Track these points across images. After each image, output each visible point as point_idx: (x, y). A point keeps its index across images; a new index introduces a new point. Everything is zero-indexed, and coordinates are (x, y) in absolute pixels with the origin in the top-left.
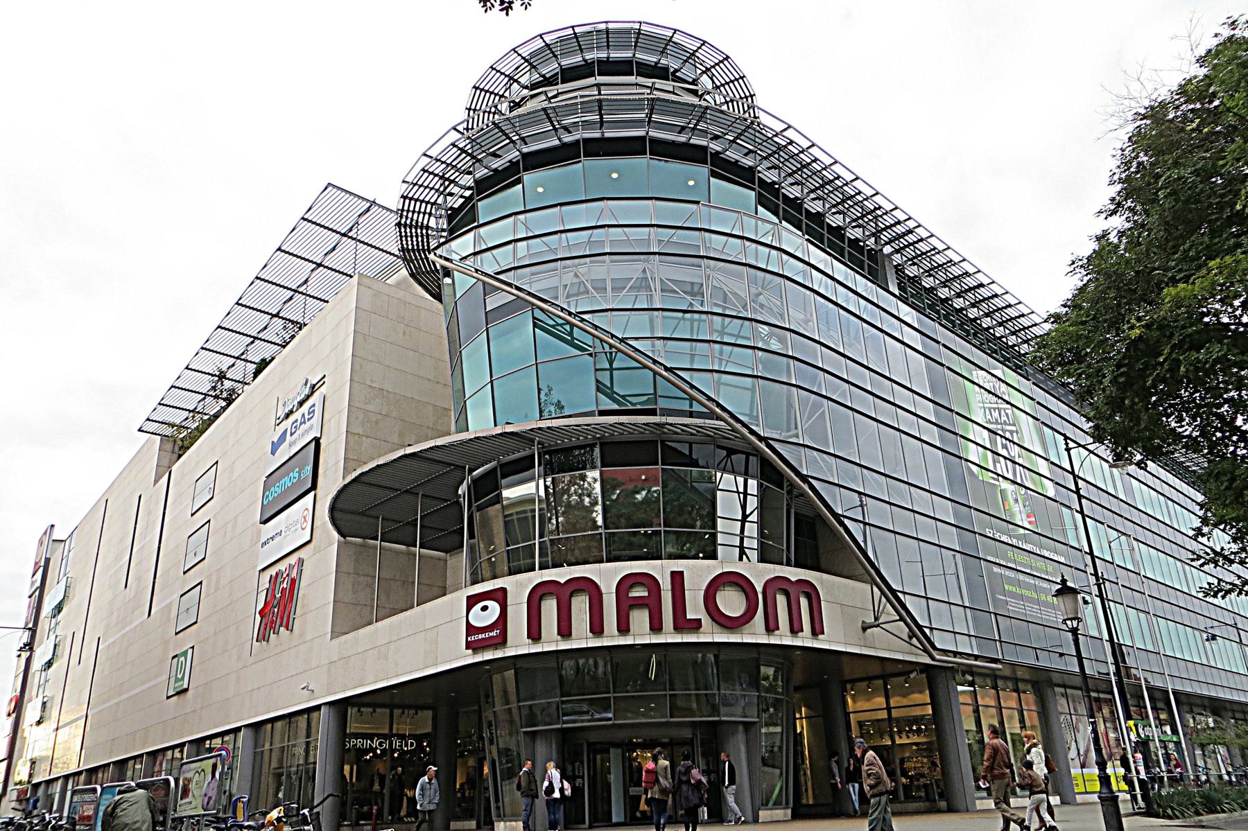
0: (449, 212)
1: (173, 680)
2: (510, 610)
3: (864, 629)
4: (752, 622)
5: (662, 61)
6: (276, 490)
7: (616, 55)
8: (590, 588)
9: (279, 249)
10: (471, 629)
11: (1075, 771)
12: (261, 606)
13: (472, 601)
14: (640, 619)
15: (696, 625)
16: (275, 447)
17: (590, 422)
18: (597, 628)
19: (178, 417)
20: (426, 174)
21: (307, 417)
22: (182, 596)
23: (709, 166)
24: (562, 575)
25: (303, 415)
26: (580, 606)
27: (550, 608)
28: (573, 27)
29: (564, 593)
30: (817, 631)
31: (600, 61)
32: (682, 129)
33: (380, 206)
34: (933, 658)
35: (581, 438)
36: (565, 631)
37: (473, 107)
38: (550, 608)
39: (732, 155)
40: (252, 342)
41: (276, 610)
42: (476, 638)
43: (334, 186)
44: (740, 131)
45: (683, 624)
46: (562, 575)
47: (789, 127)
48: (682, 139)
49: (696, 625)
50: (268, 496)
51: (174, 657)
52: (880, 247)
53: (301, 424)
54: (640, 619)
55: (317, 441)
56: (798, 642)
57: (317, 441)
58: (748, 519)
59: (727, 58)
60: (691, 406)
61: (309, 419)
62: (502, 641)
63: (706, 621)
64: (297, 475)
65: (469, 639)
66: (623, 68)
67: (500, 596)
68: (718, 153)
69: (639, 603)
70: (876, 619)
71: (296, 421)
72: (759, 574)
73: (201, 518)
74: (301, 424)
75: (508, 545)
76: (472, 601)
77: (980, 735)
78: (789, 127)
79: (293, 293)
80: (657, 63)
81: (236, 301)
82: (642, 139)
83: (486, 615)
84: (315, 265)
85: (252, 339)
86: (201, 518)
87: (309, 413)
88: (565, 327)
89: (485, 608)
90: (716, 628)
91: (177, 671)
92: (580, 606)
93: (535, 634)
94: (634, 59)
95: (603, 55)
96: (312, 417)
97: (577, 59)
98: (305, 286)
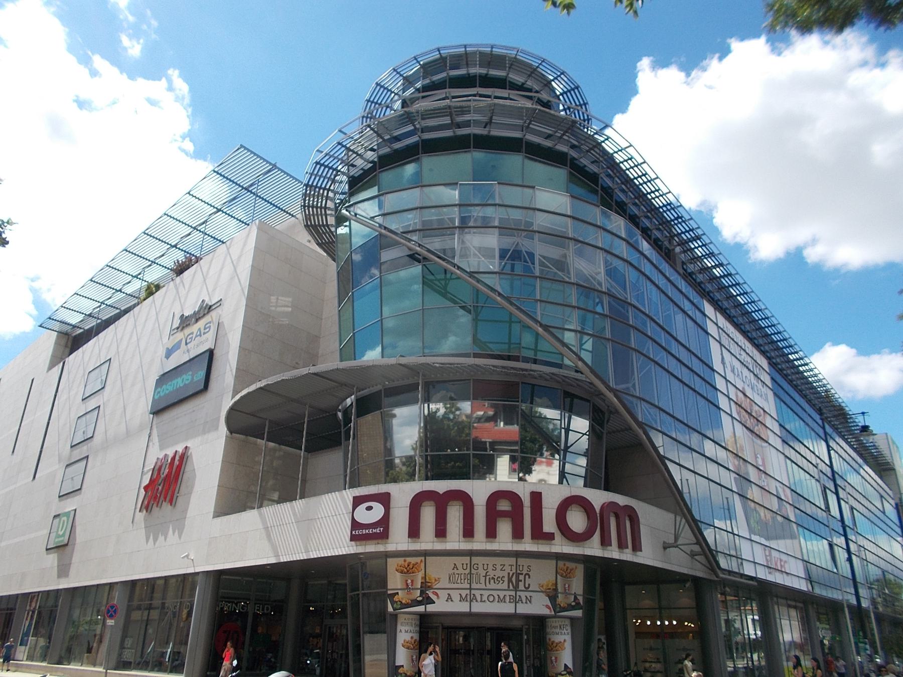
0: (350, 179)
1: (53, 535)
2: (394, 513)
3: (665, 548)
4: (592, 539)
5: (528, 83)
6: (169, 388)
7: (494, 72)
8: (465, 500)
9: (189, 193)
10: (355, 525)
11: (785, 663)
12: (146, 481)
13: (358, 501)
14: (504, 528)
15: (550, 537)
16: (169, 353)
17: (453, 362)
18: (468, 532)
19: (74, 319)
20: (340, 146)
21: (202, 331)
22: (68, 466)
23: (568, 168)
24: (441, 486)
25: (199, 329)
26: (455, 514)
27: (428, 514)
28: (465, 46)
29: (442, 502)
30: (637, 547)
31: (481, 76)
32: (548, 137)
33: (279, 169)
34: (717, 576)
35: (451, 374)
36: (441, 532)
37: (372, 99)
38: (428, 514)
39: (584, 161)
40: (150, 265)
41: (160, 488)
42: (358, 532)
43: (245, 148)
44: (591, 146)
45: (539, 534)
46: (441, 486)
47: (631, 146)
48: (548, 143)
49: (550, 537)
50: (159, 392)
51: (55, 517)
52: (673, 247)
53: (196, 336)
54: (504, 528)
55: (211, 353)
56: (607, 554)
57: (211, 353)
58: (569, 450)
59: (577, 87)
60: (535, 355)
61: (204, 333)
62: (384, 536)
63: (558, 536)
64: (190, 378)
65: (353, 533)
66: (501, 83)
67: (385, 499)
68: (574, 158)
69: (504, 514)
70: (676, 539)
71: (192, 333)
72: (598, 498)
73: (92, 404)
74: (196, 336)
75: (385, 457)
76: (358, 501)
77: (729, 632)
78: (631, 146)
79: (192, 229)
80: (523, 84)
81: (143, 231)
82: (521, 140)
83: (371, 514)
84: (215, 210)
85: (150, 263)
86: (92, 404)
87: (205, 329)
88: (441, 282)
89: (369, 508)
90: (565, 541)
91: (58, 528)
92: (455, 514)
93: (414, 532)
94: (508, 79)
95: (483, 71)
96: (208, 332)
97: (462, 72)
98: (204, 225)
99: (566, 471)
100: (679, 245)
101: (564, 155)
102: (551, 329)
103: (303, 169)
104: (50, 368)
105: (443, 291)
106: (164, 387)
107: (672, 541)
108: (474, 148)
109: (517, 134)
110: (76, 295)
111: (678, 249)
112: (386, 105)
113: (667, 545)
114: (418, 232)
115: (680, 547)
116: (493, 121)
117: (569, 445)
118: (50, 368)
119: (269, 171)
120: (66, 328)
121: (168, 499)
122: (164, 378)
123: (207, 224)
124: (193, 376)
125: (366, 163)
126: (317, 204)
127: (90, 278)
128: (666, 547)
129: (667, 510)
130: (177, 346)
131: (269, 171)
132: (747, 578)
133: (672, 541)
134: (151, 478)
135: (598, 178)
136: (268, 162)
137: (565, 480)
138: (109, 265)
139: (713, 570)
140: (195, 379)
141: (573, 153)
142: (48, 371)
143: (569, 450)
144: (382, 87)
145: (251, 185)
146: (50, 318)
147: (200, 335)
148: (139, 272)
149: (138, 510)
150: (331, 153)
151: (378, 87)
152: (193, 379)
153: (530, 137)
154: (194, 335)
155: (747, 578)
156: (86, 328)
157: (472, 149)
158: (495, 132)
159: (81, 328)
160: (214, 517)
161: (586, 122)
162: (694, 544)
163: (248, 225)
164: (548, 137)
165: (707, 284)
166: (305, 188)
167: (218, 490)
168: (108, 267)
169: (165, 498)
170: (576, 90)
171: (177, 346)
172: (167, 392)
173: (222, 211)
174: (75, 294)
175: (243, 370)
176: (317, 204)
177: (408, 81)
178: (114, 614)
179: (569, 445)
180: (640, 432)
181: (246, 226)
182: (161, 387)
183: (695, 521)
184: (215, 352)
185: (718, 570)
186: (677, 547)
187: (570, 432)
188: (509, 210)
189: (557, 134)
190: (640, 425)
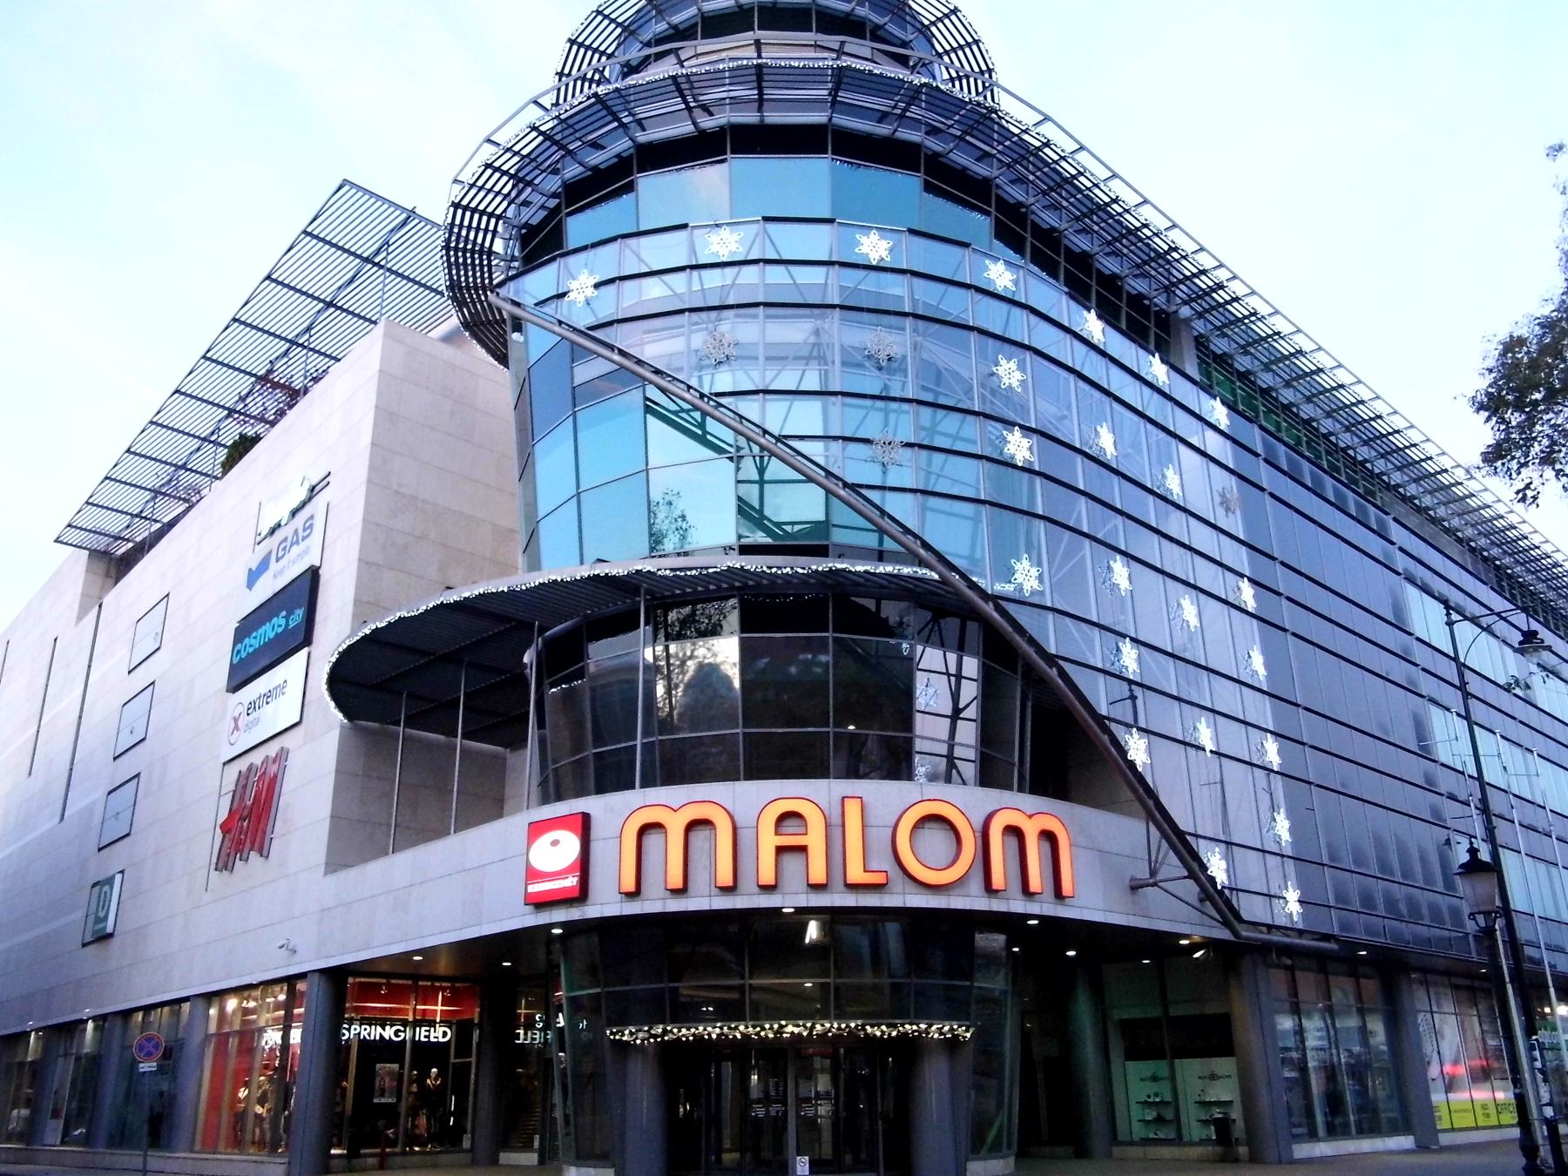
0: (523, 231)
1: (91, 919)
6: (253, 642)
9: (268, 277)
16: (253, 577)
19: (115, 524)
21: (301, 534)
25: (296, 532)
32: (883, 117)
33: (422, 219)
43: (353, 185)
48: (883, 130)
50: (239, 652)
51: (94, 886)
52: (1174, 308)
58: (961, 716)
64: (283, 622)
67: (584, 825)
70: (1153, 873)
71: (285, 540)
96: (309, 535)
98: (307, 336)
99: (955, 755)
100: (1185, 303)
101: (916, 147)
102: (863, 491)
103: (439, 212)
104: (80, 618)
105: (700, 432)
106: (247, 641)
107: (1143, 873)
108: (732, 153)
109: (817, 117)
110: (108, 481)
111: (1185, 312)
112: (581, 74)
113: (1137, 883)
114: (687, 313)
115: (1160, 884)
116: (765, 97)
117: (961, 706)
118: (80, 618)
119: (404, 224)
120: (101, 543)
121: (257, 845)
122: (245, 628)
123: (313, 332)
124: (287, 618)
125: (545, 198)
126: (483, 281)
127: (126, 448)
128: (1135, 887)
129: (1130, 814)
130: (264, 565)
131: (404, 224)
132: (1315, 937)
133: (1143, 873)
134: (231, 809)
135: (991, 186)
136: (398, 206)
137: (954, 771)
138: (154, 420)
139: (1226, 923)
140: (292, 625)
141: (933, 144)
142: (77, 624)
143: (961, 716)
144: (581, 45)
145: (377, 252)
146: (69, 525)
147: (297, 543)
148: (211, 430)
149: (213, 867)
150: (480, 183)
151: (575, 48)
152: (287, 624)
153: (843, 121)
154: (288, 544)
155: (1315, 937)
156: (138, 539)
157: (729, 156)
158: (774, 117)
159: (128, 540)
160: (224, 863)
161: (987, 76)
162: (1185, 877)
163: (375, 323)
164: (883, 117)
165: (1260, 374)
166: (444, 252)
167: (331, 823)
168: (154, 426)
169: (253, 843)
170: (953, 18)
171: (264, 565)
172: (251, 650)
173: (335, 306)
174: (106, 478)
175: (368, 603)
176: (483, 281)
177: (629, 31)
178: (153, 1043)
179: (961, 706)
180: (1054, 672)
181: (372, 326)
182: (242, 643)
183: (1181, 835)
184: (321, 571)
185: (1235, 923)
186: (1155, 884)
187: (963, 680)
188: (794, 269)
189: (896, 111)
190: (1051, 660)
